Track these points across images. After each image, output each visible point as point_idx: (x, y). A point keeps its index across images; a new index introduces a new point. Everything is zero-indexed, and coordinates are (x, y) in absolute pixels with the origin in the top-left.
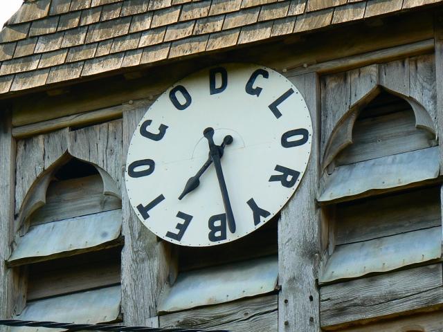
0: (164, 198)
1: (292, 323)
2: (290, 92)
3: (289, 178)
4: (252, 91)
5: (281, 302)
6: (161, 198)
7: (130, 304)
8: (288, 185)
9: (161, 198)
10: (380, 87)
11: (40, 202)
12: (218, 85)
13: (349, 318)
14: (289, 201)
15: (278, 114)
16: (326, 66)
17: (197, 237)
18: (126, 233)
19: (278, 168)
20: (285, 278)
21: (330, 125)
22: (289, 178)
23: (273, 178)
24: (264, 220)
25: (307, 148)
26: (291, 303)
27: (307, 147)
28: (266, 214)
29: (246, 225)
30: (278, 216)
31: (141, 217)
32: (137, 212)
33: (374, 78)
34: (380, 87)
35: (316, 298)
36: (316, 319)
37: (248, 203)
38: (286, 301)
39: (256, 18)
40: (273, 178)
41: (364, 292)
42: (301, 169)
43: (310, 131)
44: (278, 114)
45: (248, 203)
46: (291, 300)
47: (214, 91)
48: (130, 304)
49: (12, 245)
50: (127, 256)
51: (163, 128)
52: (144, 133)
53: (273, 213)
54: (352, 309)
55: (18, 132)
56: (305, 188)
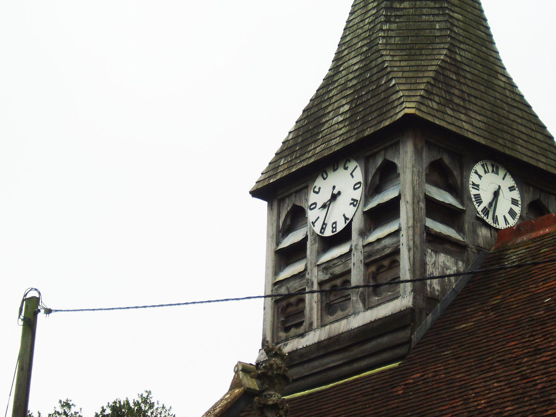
0: (509, 188)
1: (355, 264)
2: (357, 166)
3: (355, 203)
4: (346, 168)
5: (352, 255)
6: (318, 218)
7: (309, 263)
8: (355, 206)
9: (318, 218)
10: (294, 204)
11: (288, 225)
12: (325, 176)
13: (373, 258)
14: (355, 213)
15: (353, 177)
16: (368, 153)
17: (328, 233)
18: (308, 234)
19: (352, 199)
20: (354, 244)
21: (370, 178)
22: (355, 203)
23: (351, 204)
24: (348, 222)
25: (360, 190)
26: (355, 255)
27: (361, 189)
28: (348, 219)
29: (341, 226)
30: (352, 220)
31: (313, 226)
32: (311, 224)
33: (383, 156)
34: (294, 204)
35: (362, 252)
36: (362, 261)
37: (510, 191)
38: (354, 254)
39: (437, 63)
40: (351, 204)
41: (378, 247)
42: (359, 199)
43: (362, 182)
44: (353, 177)
45: (510, 191)
46: (355, 253)
47: (325, 179)
48: (309, 263)
49: (278, 244)
50: (309, 243)
51: (320, 188)
52: (315, 192)
53: (350, 218)
54: (373, 254)
55: (279, 197)
56: (360, 207)
